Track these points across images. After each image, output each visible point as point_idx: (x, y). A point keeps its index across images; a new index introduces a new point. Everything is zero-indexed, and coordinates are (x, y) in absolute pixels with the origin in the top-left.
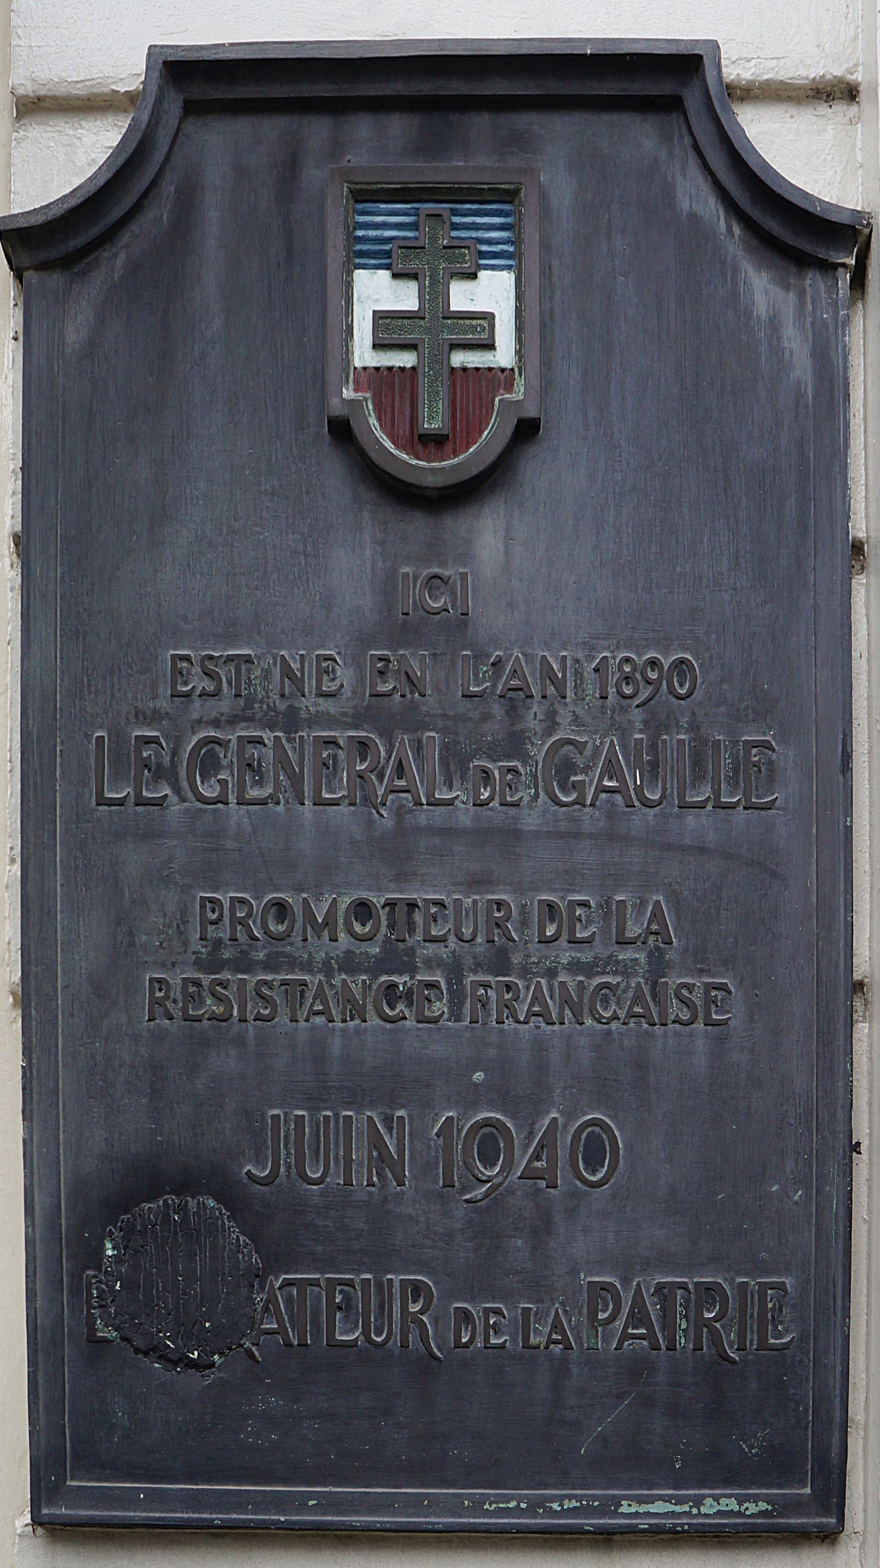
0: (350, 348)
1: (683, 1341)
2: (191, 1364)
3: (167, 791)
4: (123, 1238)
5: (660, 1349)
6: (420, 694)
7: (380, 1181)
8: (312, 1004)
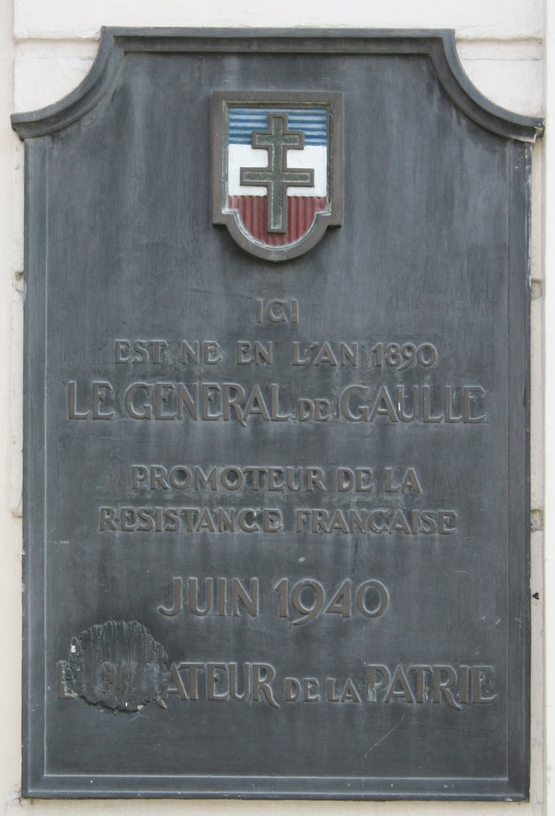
0: (226, 186)
1: (427, 697)
2: (125, 710)
3: (113, 412)
4: (82, 643)
5: (412, 702)
6: (267, 363)
7: (241, 613)
8: (201, 522)
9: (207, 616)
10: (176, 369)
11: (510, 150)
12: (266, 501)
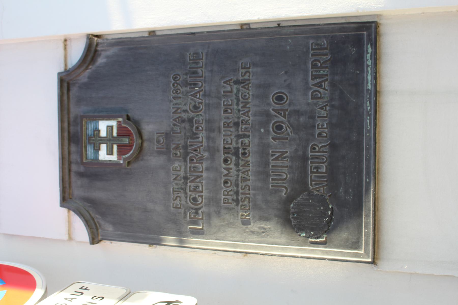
9: (288, 174)
10: (183, 184)
11: (99, 48)
12: (237, 146)
